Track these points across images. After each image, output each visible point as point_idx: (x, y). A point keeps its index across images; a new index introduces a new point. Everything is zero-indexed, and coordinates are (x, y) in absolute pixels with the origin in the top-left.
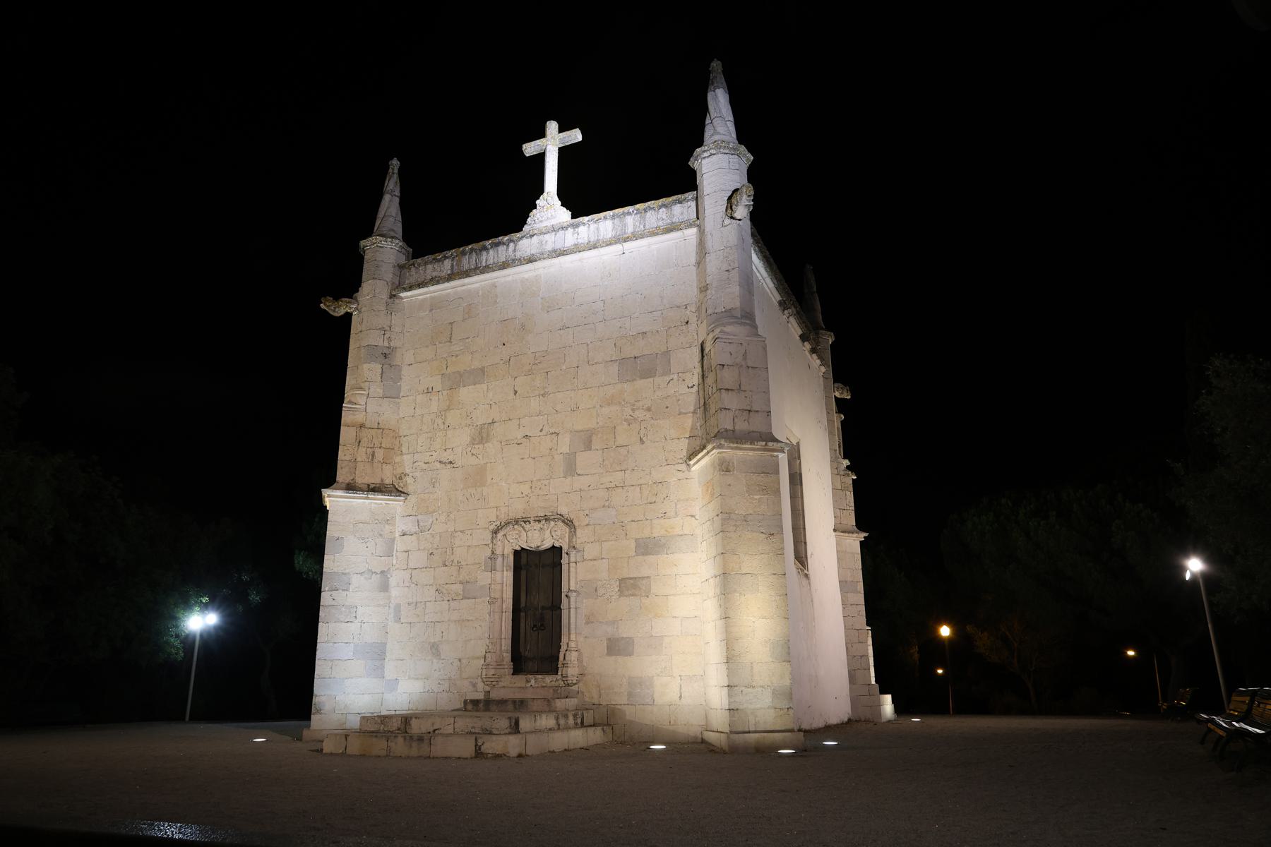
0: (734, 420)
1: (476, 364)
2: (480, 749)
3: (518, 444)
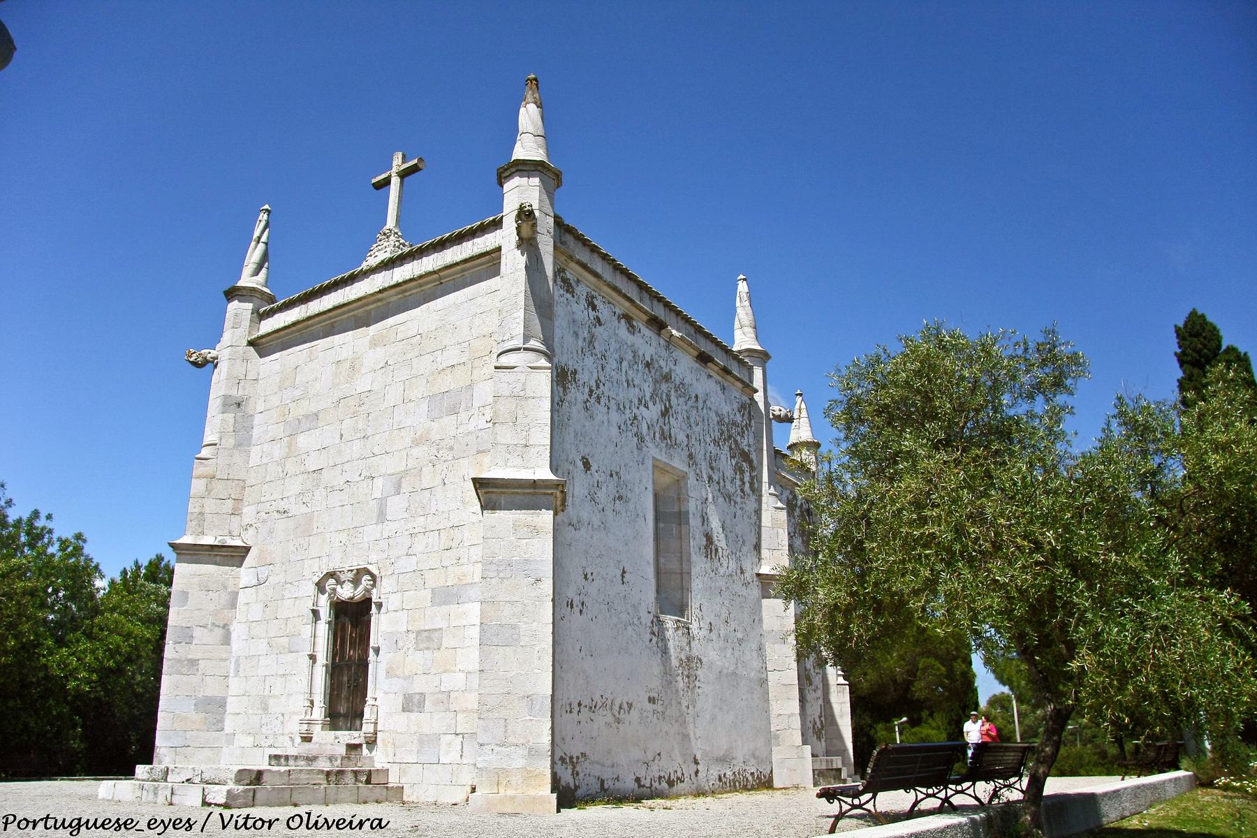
1: (313, 409)
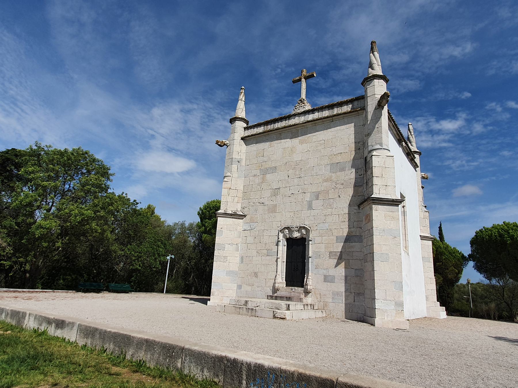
2: (275, 315)
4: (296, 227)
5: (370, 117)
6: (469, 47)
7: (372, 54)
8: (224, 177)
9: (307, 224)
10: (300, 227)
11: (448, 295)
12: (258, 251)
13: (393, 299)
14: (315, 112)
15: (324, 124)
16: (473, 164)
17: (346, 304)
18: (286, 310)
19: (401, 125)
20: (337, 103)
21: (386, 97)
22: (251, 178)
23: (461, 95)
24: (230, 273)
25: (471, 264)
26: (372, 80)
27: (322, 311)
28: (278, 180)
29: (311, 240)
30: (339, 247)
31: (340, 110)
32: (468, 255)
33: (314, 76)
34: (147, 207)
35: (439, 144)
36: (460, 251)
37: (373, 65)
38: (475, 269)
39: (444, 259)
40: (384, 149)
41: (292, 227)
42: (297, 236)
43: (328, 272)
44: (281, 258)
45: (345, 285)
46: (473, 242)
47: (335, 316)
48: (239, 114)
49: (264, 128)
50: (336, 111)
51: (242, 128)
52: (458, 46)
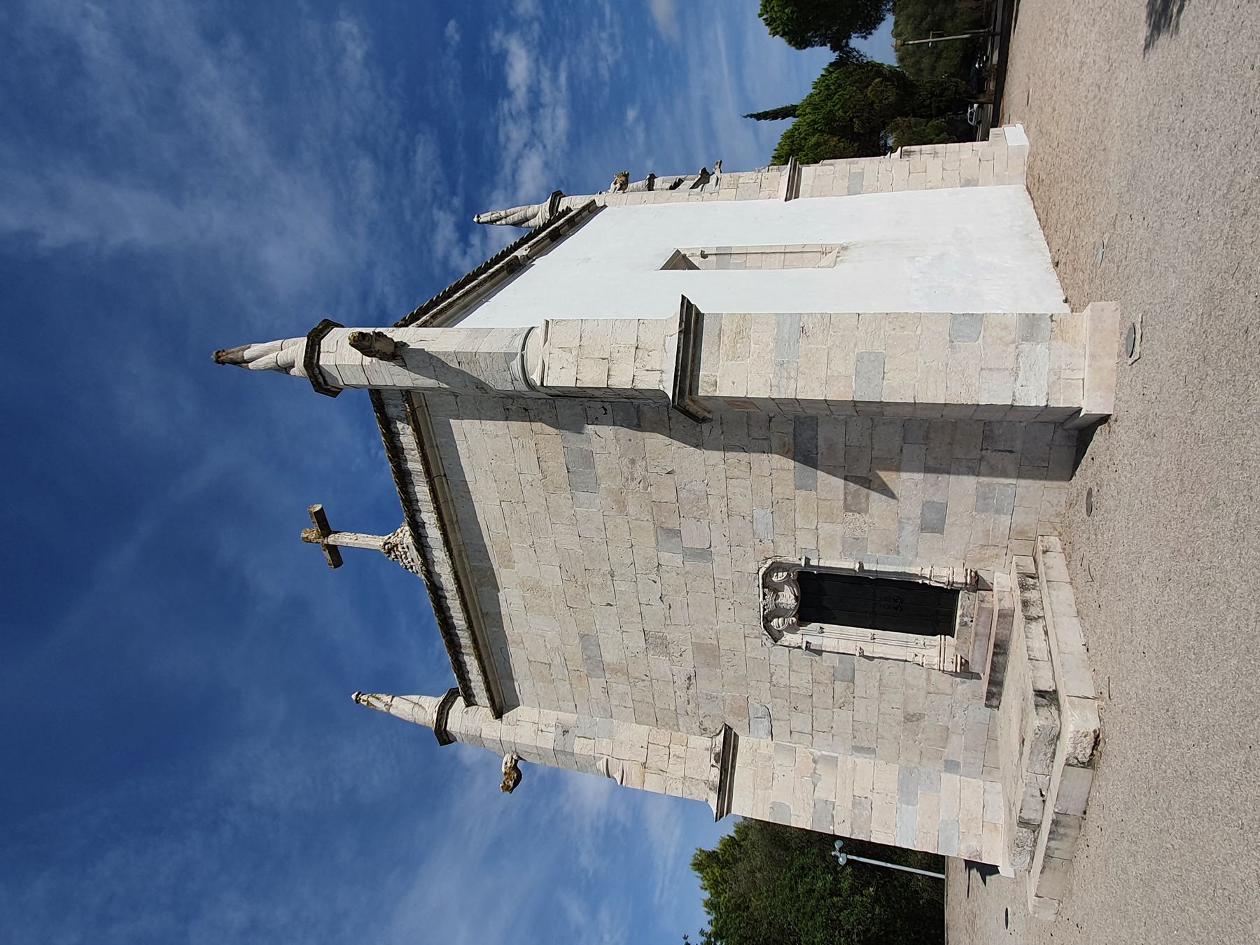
0: (648, 370)
2: (1083, 763)
3: (670, 607)
4: (764, 599)
5: (430, 383)
6: (347, 26)
7: (250, 365)
8: (609, 776)
9: (754, 567)
10: (763, 588)
11: (936, 95)
12: (836, 706)
13: (1014, 346)
14: (420, 521)
15: (455, 500)
16: (608, 15)
17: (1020, 476)
18: (1059, 709)
19: (517, 177)
20: (391, 460)
21: (366, 343)
22: (614, 702)
23: (453, 43)
24: (907, 791)
25: (856, 42)
26: (322, 370)
27: (1045, 552)
28: (619, 633)
29: (808, 560)
30: (831, 486)
31: (413, 453)
32: (834, 52)
33: (322, 508)
34: (697, 873)
35: (561, 92)
36: (823, 73)
37: (279, 363)
38: (871, 34)
39: (845, 113)
40: (523, 349)
41: (765, 610)
42: (793, 597)
43: (909, 519)
44: (859, 644)
45: (954, 474)
46: (799, 39)
47: (1059, 509)
48: (429, 717)
49: (467, 654)
50: (414, 465)
51: (467, 712)
52: (344, 49)
